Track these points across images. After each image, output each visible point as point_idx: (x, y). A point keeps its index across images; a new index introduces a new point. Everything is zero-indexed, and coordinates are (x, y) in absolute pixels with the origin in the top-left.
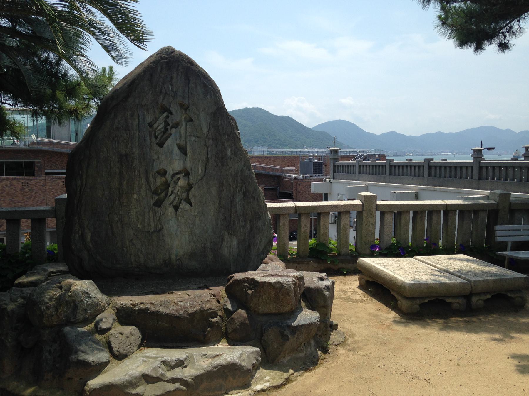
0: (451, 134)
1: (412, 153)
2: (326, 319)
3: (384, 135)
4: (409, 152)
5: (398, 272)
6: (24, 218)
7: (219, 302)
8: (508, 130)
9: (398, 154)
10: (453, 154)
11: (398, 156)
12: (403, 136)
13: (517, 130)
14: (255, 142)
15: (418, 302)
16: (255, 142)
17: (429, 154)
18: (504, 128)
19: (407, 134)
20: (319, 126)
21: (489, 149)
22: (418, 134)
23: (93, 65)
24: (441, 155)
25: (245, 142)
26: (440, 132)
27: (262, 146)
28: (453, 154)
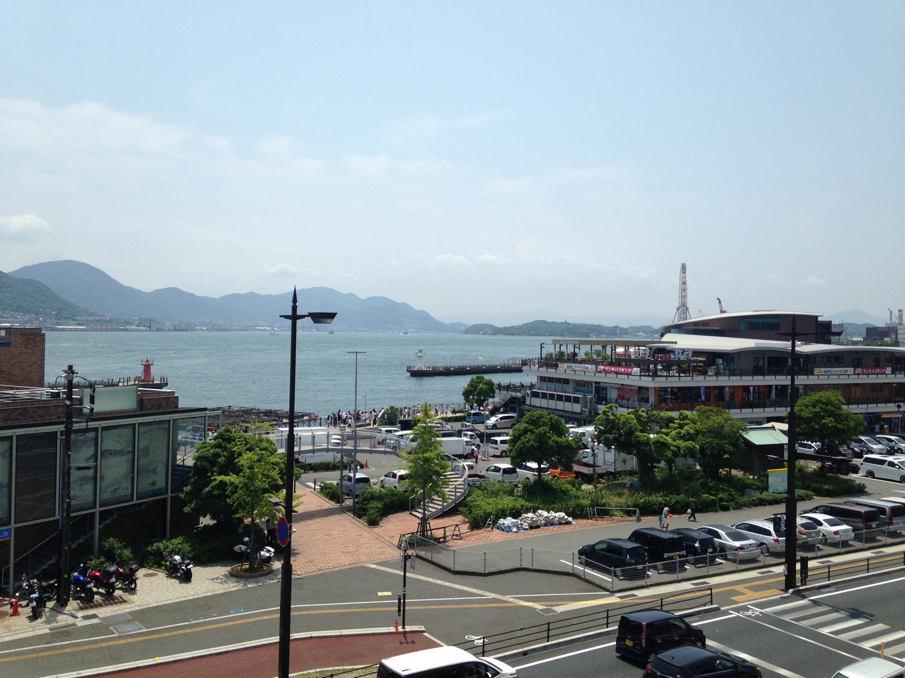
0: (270, 297)
1: (207, 325)
2: (151, 564)
3: (158, 292)
4: (202, 324)
5: (384, 435)
6: (735, 408)
7: (406, 425)
8: (351, 295)
9: (183, 327)
10: (273, 329)
11: (182, 330)
12: (192, 296)
13: (363, 296)
15: (464, 382)
17: (235, 328)
18: (345, 291)
19: (198, 293)
21: (320, 317)
22: (217, 295)
23: (92, 314)
24: (254, 330)
26: (176, 289)
28: (273, 329)
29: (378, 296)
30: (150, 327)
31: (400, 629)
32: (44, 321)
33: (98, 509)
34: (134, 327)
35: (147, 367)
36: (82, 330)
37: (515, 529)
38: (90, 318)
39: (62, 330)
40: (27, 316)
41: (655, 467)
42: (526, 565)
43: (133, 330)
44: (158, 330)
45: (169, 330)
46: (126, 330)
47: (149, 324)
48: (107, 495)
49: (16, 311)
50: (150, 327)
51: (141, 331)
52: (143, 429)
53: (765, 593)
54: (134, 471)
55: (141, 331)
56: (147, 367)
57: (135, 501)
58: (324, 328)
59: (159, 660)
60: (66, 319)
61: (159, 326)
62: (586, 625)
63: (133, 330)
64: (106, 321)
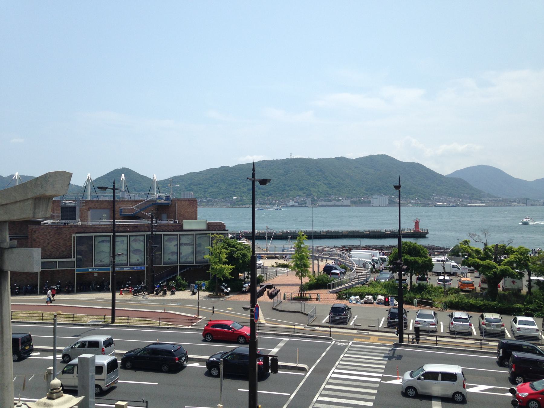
14: (378, 190)
16: (378, 190)
20: (457, 172)
21: (264, 182)
25: (367, 191)
27: (385, 194)
29: (217, 166)
30: (526, 204)
31: (196, 316)
32: (462, 201)
33: (179, 265)
34: (516, 204)
35: (417, 223)
36: (482, 206)
37: (354, 302)
38: (490, 199)
39: (471, 206)
40: (453, 199)
41: (318, 260)
42: (303, 311)
43: (515, 206)
44: (532, 205)
45: (540, 205)
46: (510, 206)
47: (526, 202)
48: (182, 260)
49: (448, 196)
50: (526, 204)
51: (521, 206)
52: (198, 236)
53: (359, 340)
54: (195, 253)
55: (521, 206)
56: (417, 223)
57: (195, 264)
58: (268, 187)
59: (125, 309)
60: (475, 199)
61: (533, 203)
62: (366, 353)
63: (515, 206)
64: (500, 201)
